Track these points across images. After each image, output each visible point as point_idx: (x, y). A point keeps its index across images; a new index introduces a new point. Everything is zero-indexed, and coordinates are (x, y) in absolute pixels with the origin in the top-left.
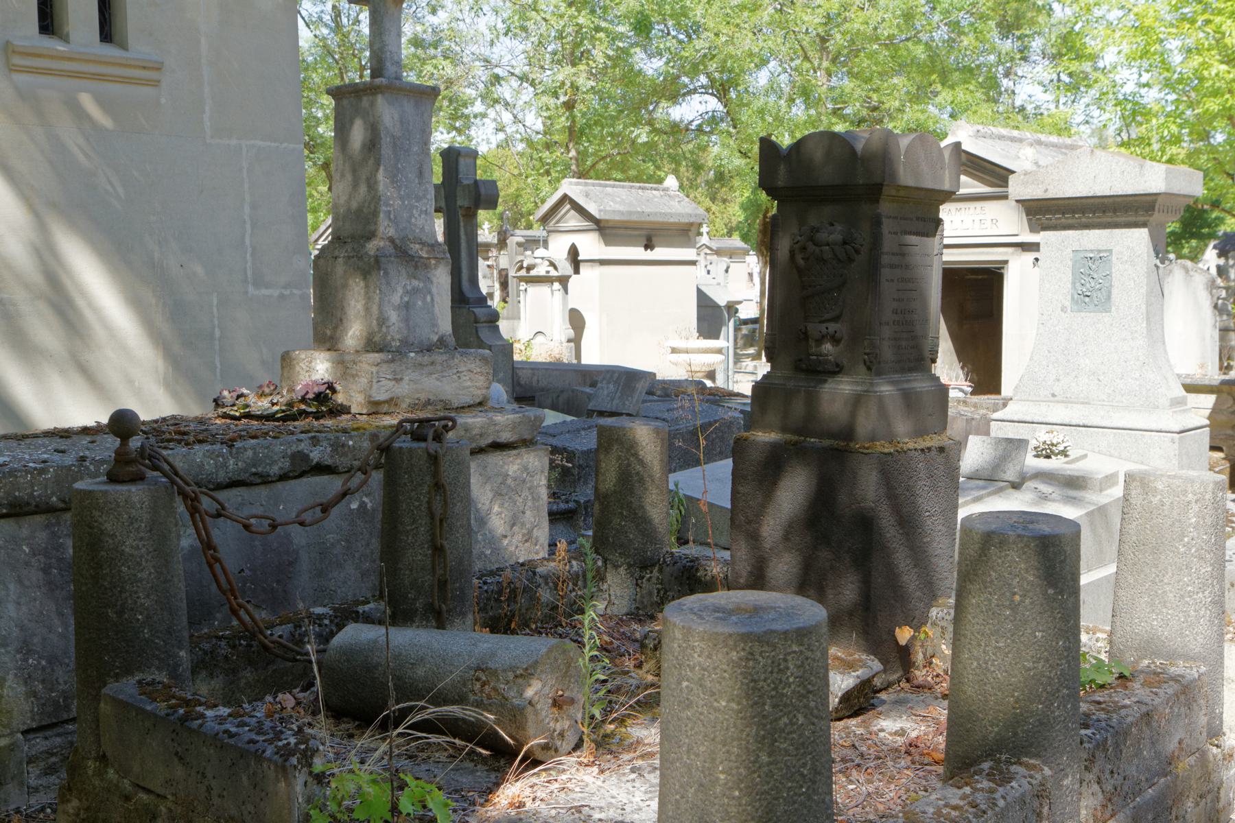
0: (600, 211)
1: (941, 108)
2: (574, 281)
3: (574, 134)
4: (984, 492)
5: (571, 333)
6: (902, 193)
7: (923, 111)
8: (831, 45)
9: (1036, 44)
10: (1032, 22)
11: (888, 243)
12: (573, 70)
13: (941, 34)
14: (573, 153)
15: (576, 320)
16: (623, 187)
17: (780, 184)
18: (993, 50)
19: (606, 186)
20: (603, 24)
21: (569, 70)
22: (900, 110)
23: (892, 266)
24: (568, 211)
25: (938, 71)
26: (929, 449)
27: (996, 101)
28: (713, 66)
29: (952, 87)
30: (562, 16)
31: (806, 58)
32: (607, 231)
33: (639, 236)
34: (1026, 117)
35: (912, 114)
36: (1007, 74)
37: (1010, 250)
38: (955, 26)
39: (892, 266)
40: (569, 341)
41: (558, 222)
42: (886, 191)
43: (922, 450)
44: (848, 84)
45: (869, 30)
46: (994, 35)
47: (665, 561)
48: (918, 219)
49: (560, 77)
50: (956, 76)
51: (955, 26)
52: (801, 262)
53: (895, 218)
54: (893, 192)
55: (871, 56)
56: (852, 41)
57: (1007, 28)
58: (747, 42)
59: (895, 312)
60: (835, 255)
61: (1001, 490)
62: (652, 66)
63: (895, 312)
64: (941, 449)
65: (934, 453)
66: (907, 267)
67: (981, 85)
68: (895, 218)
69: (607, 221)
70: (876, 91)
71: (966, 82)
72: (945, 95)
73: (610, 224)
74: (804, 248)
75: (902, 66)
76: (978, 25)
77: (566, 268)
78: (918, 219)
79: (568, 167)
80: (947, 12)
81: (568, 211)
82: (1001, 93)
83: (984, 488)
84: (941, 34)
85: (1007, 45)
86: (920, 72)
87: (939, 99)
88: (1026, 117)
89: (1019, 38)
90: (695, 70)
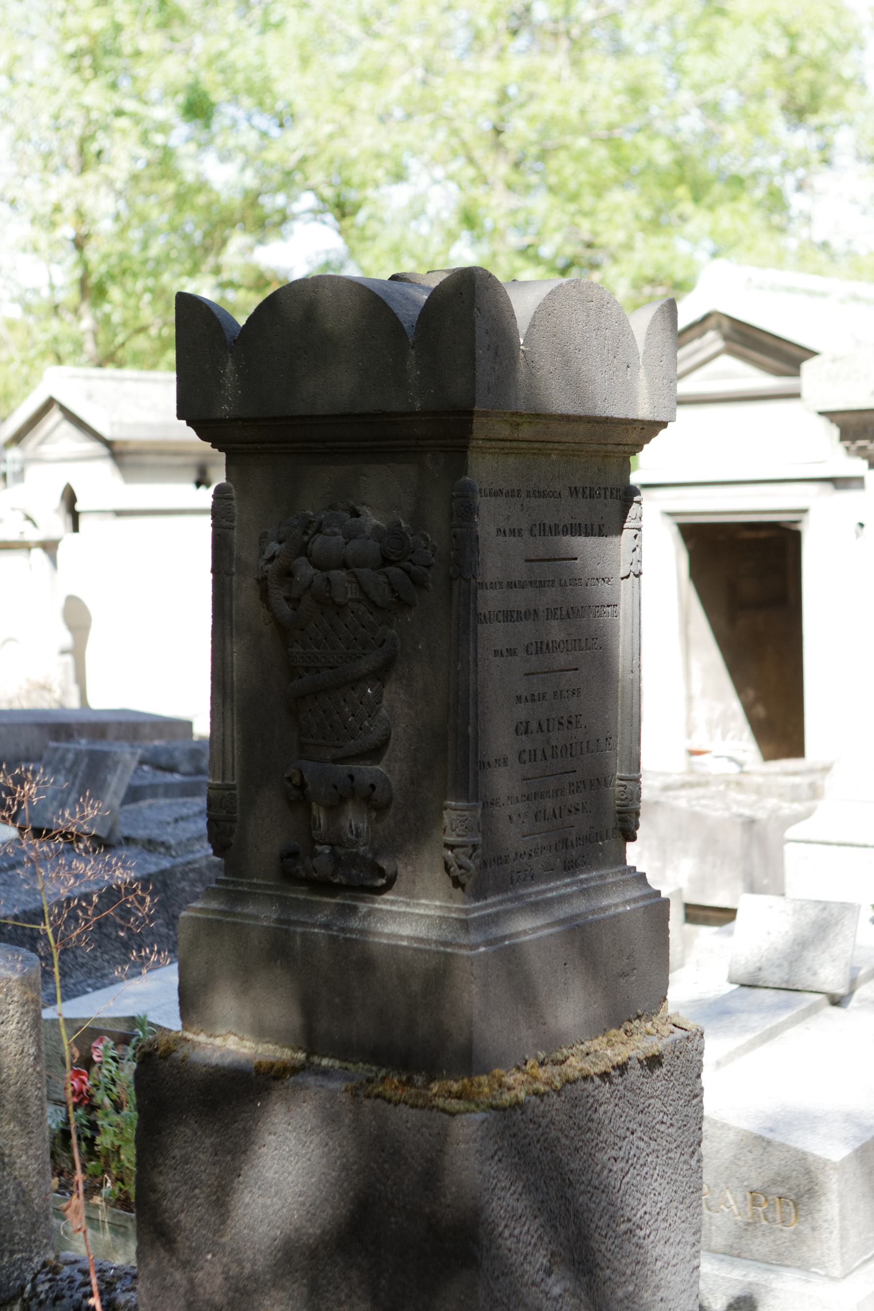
0: (112, 424)
1: (695, 242)
2: (70, 545)
3: (92, 290)
4: (783, 1017)
5: (66, 639)
6: (526, 431)
7: (664, 248)
8: (511, 142)
9: (844, 140)
10: (837, 104)
11: (499, 556)
12: (78, 183)
13: (692, 123)
14: (87, 323)
15: (76, 617)
16: (155, 381)
17: (225, 410)
18: (775, 148)
19: (123, 380)
20: (130, 105)
21: (67, 180)
22: (628, 246)
23: (509, 616)
24: (57, 425)
25: (690, 180)
26: (622, 1068)
27: (782, 230)
28: (317, 177)
29: (711, 208)
30: (55, 90)
31: (471, 161)
32: (128, 459)
33: (185, 466)
34: (833, 258)
35: (648, 253)
36: (800, 187)
37: (814, 488)
38: (712, 110)
39: (509, 616)
40: (63, 652)
41: (41, 442)
42: (481, 427)
43: (605, 1076)
44: (540, 203)
45: (573, 114)
46: (778, 124)
47: (34, 1294)
48: (574, 492)
49: (53, 196)
50: (717, 189)
51: (712, 110)
52: (286, 609)
53: (512, 494)
54: (505, 431)
55: (580, 157)
56: (544, 133)
57: (798, 112)
58: (367, 136)
59: (522, 729)
60: (366, 594)
61: (813, 1010)
62: (224, 177)
63: (522, 729)
64: (653, 1062)
65: (635, 1073)
66: (575, 581)
67: (758, 204)
68: (512, 494)
69: (125, 443)
70: (588, 214)
71: (734, 198)
72: (699, 220)
73: (131, 447)
74: (287, 574)
75: (627, 174)
76: (753, 107)
77: (54, 524)
78: (574, 492)
79: (78, 346)
80: (698, 88)
81: (57, 425)
82: (790, 219)
83: (787, 1006)
84: (692, 123)
85: (801, 140)
86: (663, 185)
87: (690, 228)
88: (833, 258)
89: (820, 129)
90: (288, 180)
